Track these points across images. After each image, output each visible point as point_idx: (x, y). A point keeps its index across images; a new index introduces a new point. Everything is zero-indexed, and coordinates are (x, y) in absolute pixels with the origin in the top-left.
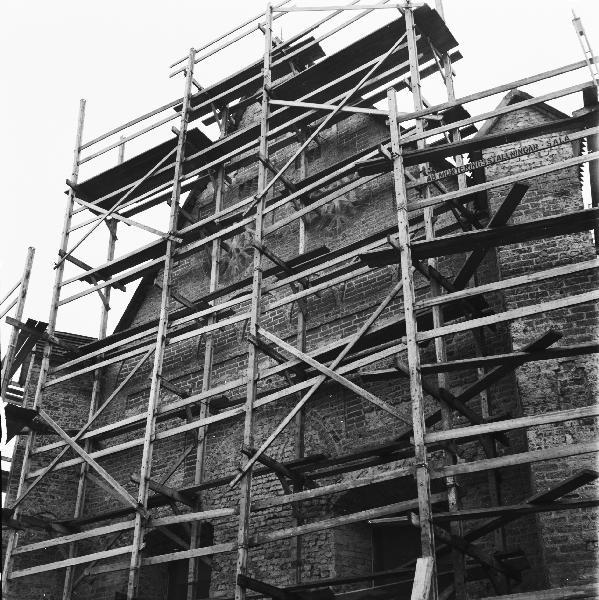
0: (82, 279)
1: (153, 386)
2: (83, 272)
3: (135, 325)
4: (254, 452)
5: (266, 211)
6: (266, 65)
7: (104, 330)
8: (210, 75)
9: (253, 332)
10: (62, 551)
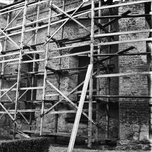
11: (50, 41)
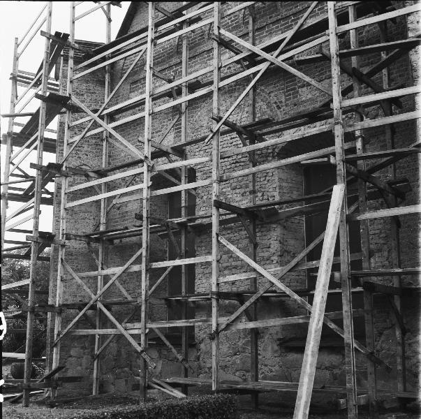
4: (221, 118)
10: (97, 189)
11: (221, 131)
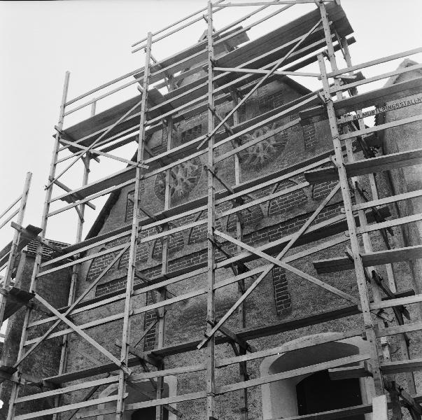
0: (63, 199)
1: (129, 275)
2: (65, 193)
3: (100, 235)
4: (216, 323)
5: (216, 145)
6: (146, 75)
7: (80, 238)
8: (163, 52)
9: (211, 233)
10: (50, 402)
11: (215, 336)
